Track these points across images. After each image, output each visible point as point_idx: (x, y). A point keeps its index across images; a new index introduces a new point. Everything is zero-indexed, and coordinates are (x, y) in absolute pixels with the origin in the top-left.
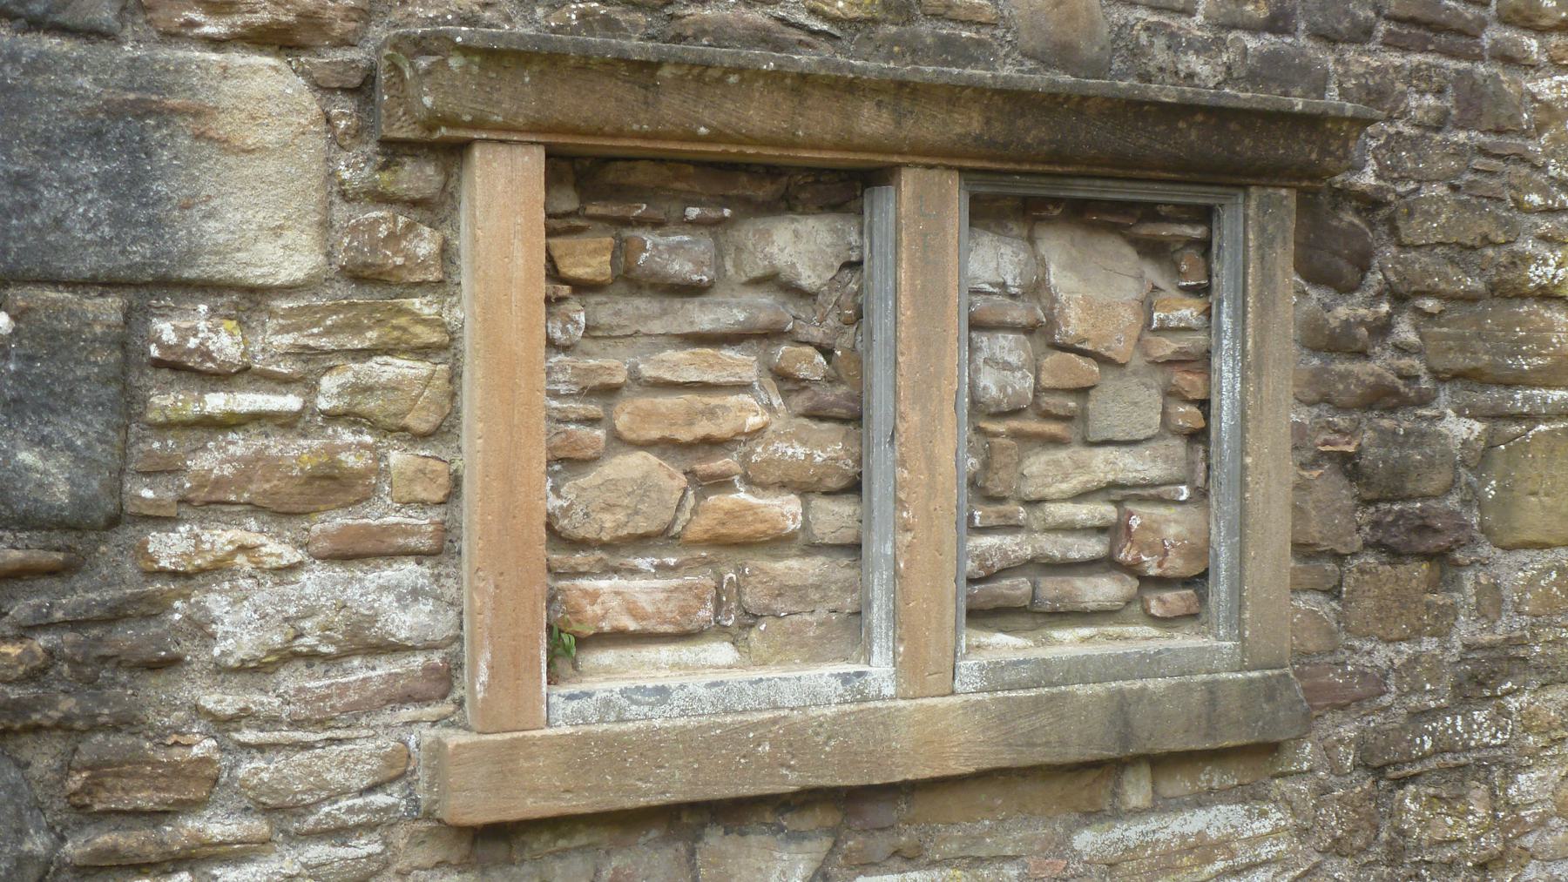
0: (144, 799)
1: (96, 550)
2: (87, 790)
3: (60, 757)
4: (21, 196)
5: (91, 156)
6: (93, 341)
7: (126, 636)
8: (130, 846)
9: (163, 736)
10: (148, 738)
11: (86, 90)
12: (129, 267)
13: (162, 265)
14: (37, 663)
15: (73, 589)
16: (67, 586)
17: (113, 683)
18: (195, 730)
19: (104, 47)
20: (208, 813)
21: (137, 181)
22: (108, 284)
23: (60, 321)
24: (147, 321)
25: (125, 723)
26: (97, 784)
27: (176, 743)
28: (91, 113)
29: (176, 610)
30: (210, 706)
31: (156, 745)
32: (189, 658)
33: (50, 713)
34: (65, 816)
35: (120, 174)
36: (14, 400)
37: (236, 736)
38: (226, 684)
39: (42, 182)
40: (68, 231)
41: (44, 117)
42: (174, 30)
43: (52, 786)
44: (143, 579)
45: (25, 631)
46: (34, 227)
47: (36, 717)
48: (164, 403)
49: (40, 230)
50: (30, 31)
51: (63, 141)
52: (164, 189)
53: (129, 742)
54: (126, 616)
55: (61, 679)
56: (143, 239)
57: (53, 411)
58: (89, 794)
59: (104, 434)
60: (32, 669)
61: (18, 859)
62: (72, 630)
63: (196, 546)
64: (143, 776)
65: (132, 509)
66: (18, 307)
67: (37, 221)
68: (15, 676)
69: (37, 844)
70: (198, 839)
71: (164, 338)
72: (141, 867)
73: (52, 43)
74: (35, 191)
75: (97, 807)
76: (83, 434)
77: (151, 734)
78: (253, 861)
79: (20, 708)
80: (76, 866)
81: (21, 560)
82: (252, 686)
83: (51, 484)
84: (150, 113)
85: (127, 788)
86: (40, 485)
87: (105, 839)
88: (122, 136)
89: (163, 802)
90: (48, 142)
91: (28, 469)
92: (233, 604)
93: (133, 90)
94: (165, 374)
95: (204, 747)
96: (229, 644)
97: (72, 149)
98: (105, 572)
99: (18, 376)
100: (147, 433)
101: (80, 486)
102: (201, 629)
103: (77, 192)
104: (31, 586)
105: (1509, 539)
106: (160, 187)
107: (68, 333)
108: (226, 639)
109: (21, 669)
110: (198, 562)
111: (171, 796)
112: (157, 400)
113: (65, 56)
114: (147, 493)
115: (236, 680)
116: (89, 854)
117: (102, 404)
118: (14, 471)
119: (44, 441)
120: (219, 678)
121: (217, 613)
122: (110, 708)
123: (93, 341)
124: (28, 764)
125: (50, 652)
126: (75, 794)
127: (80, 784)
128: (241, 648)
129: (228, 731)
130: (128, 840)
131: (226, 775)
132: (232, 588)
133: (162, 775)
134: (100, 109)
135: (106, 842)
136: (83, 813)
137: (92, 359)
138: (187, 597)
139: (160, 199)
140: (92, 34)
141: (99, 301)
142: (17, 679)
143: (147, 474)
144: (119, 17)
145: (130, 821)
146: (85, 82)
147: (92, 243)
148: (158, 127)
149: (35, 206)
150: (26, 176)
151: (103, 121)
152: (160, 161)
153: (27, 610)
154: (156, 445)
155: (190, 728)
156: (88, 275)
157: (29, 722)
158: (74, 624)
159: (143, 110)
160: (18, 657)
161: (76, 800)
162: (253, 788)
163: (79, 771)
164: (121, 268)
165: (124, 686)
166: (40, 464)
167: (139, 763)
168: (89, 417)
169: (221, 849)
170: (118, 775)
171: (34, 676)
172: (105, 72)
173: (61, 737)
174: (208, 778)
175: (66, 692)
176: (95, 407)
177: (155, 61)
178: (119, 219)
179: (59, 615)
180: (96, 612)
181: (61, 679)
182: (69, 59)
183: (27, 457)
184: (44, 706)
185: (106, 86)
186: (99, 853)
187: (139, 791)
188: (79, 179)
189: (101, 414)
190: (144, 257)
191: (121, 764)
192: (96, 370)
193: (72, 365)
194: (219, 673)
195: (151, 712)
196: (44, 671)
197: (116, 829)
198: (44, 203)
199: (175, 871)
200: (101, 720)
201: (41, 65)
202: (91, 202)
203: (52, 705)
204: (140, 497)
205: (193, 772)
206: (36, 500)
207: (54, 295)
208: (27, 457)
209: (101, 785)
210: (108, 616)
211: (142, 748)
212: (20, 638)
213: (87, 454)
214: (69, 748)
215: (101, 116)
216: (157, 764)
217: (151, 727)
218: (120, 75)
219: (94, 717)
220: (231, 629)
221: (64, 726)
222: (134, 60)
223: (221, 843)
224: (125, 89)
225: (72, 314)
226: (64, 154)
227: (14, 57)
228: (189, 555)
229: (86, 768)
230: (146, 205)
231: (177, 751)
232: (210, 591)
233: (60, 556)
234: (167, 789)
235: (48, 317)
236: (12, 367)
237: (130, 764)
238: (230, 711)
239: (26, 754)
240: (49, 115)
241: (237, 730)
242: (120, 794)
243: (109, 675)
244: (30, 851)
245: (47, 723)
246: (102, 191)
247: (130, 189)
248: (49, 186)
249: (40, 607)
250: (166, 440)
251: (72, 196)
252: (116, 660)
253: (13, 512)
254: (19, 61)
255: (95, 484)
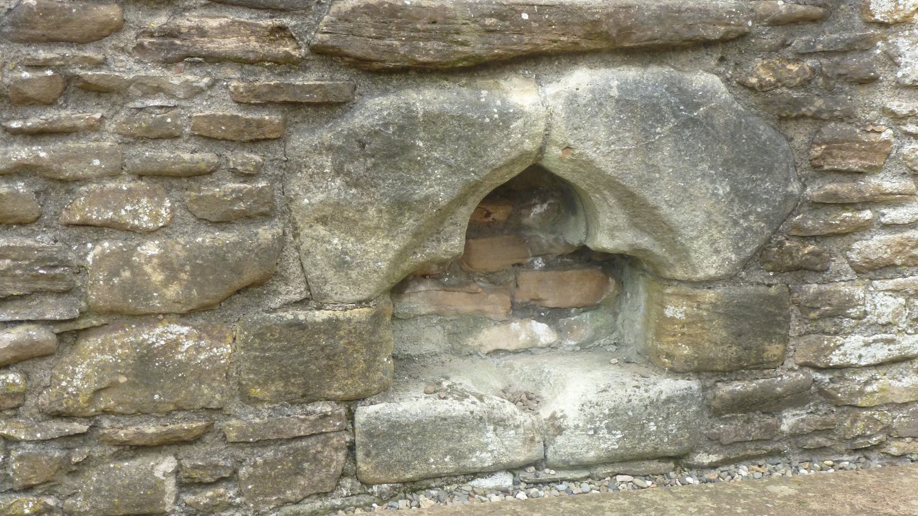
0: (854, 164)
1: (838, 7)
3: (808, 136)
7: (853, 62)
15: (824, 32)
16: (820, 30)
17: (842, 91)
18: (882, 123)
20: (881, 175)
25: (848, 117)
27: (873, 131)
30: (894, 108)
31: (862, 131)
32: (881, 78)
33: (811, 108)
34: (807, 172)
37: (904, 128)
38: (900, 95)
43: (803, 153)
44: (865, 26)
45: (800, 56)
47: (804, 110)
53: (848, 128)
54: (855, 50)
60: (804, 80)
61: (786, 196)
63: (895, 7)
64: (854, 150)
68: (795, 84)
70: (879, 190)
75: (826, 167)
78: (903, 206)
80: (813, 202)
81: (804, 11)
82: (914, 97)
85: (844, 156)
87: (831, 187)
89: (863, 166)
92: (911, 45)
95: (887, 134)
96: (907, 70)
102: (892, 60)
108: (906, 67)
109: (798, 79)
110: (896, 17)
111: (867, 163)
115: (906, 93)
116: (822, 196)
120: (897, 91)
121: (902, 50)
122: (841, 107)
124: (792, 139)
125: (813, 70)
127: (820, 152)
128: (914, 73)
129: (899, 124)
130: (842, 188)
131: (895, 152)
132: (910, 34)
133: (864, 150)
135: (832, 189)
136: (818, 171)
138: (885, 40)
142: (796, 86)
145: (841, 177)
153: (801, 43)
155: (879, 121)
157: (800, 113)
158: (826, 53)
160: (797, 72)
161: (816, 162)
162: (911, 161)
163: (819, 145)
165: (846, 94)
169: (889, 197)
170: (840, 149)
171: (805, 84)
173: (811, 123)
174: (885, 153)
175: (818, 95)
179: (819, 47)
180: (840, 46)
184: (808, 103)
186: (828, 195)
187: (851, 159)
191: (843, 142)
194: (897, 88)
195: (859, 110)
196: (809, 82)
197: (833, 182)
199: (863, 209)
200: (836, 113)
203: (811, 103)
205: (880, 149)
209: (830, 154)
210: (846, 49)
211: (855, 132)
212: (796, 61)
214: (814, 131)
216: (862, 142)
220: (909, 60)
221: (816, 118)
223: (891, 194)
228: (891, 12)
231: (872, 135)
232: (897, 36)
233: (821, 10)
237: (848, 142)
238: (905, 112)
239: (790, 133)
241: (905, 125)
242: (839, 160)
244: (792, 192)
245: (809, 114)
249: (809, 41)
252: (844, 77)
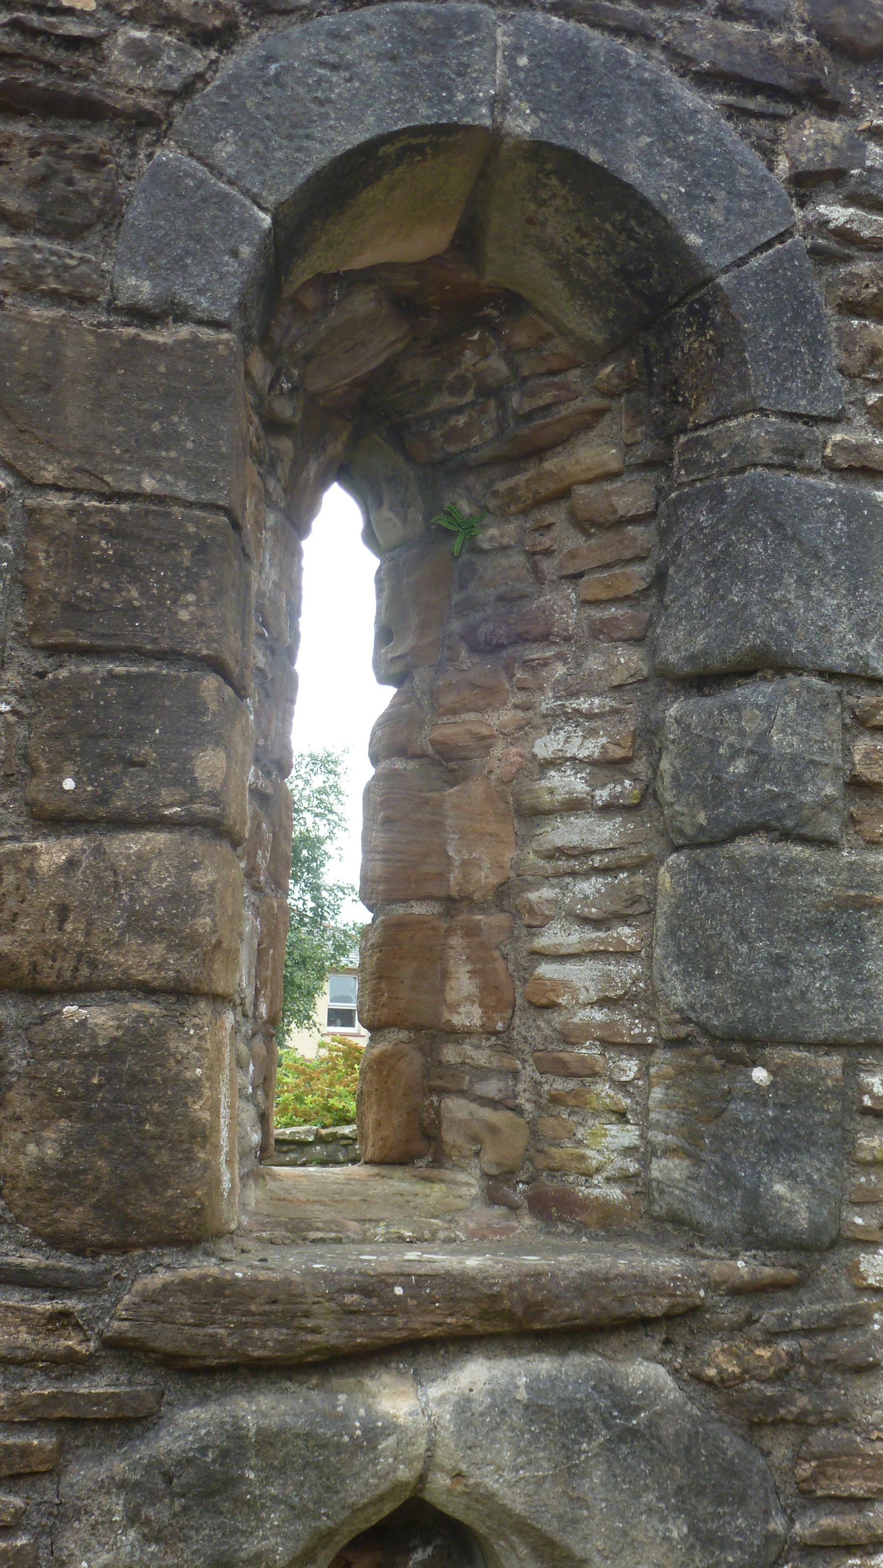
0: (857, 1487)
1: (818, 1268)
2: (813, 1478)
4: (779, 974)
5: (825, 941)
6: (826, 1092)
8: (846, 1529)
9: (867, 1432)
10: (857, 1433)
11: (822, 888)
12: (850, 1031)
13: (872, 1030)
14: (784, 1364)
19: (831, 853)
21: (856, 960)
22: (831, 1045)
23: (804, 1076)
24: (856, 1075)
25: (843, 1420)
26: (820, 1473)
28: (826, 905)
29: (875, 1322)
31: (864, 1439)
35: (844, 955)
36: (772, 1141)
39: (792, 962)
40: (809, 1002)
41: (795, 910)
42: (876, 839)
43: (786, 1473)
44: (854, 1294)
45: (771, 1337)
46: (787, 999)
47: (782, 1412)
48: (872, 1144)
49: (791, 1001)
50: (781, 840)
51: (807, 929)
52: (873, 968)
53: (845, 1436)
55: (798, 1379)
56: (861, 1009)
57: (798, 1150)
58: (815, 1481)
59: (833, 1170)
60: (780, 1370)
62: (805, 1337)
64: (856, 1466)
65: (849, 1234)
66: (776, 1064)
67: (789, 993)
69: (777, 1524)
71: (875, 1090)
72: (851, 1547)
73: (797, 850)
74: (787, 969)
75: (819, 1493)
76: (819, 1170)
77: (859, 1429)
79: (771, 1404)
80: (805, 1545)
81: (772, 1275)
83: (796, 1212)
84: (864, 906)
86: (789, 1212)
87: (828, 1522)
88: (845, 925)
89: (869, 1490)
90: (797, 930)
91: (781, 1198)
93: (852, 887)
94: (870, 1120)
97: (813, 936)
98: (825, 1287)
99: (775, 1120)
100: (856, 1169)
101: (815, 1214)
103: (816, 969)
104: (772, 1298)
105: (425, 761)
106: (870, 966)
107: (809, 1085)
109: (772, 1369)
112: (864, 1141)
113: (807, 860)
114: (859, 1221)
117: (832, 1145)
118: (770, 1200)
119: (792, 1176)
122: (832, 1406)
123: (826, 1092)
125: (791, 1355)
126: (804, 1481)
127: (809, 1472)
133: (869, 1466)
134: (832, 902)
135: (829, 1525)
137: (825, 1107)
139: (871, 975)
140: (827, 843)
141: (826, 1058)
143: (857, 1204)
144: (841, 830)
146: (820, 881)
147: (826, 1012)
148: (869, 918)
149: (788, 982)
150: (783, 958)
151: (833, 913)
152: (871, 945)
154: (863, 1180)
156: (822, 1037)
158: (807, 1332)
159: (861, 904)
160: (769, 1359)
161: (804, 1486)
163: (807, 1461)
164: (846, 1032)
166: (788, 1195)
167: (853, 1455)
168: (823, 1156)
170: (836, 1465)
171: (781, 1376)
172: (832, 873)
176: (827, 1147)
177: (867, 864)
178: (844, 992)
179: (797, 1323)
180: (825, 1322)
181: (798, 1379)
182: (809, 863)
183: (780, 1188)
185: (835, 885)
187: (852, 1479)
188: (817, 959)
189: (831, 1153)
190: (861, 1024)
192: (828, 1116)
193: (811, 1111)
195: (858, 1409)
198: (794, 979)
200: (827, 1416)
201: (791, 869)
202: (825, 978)
203: (792, 1402)
204: (854, 1223)
206: (785, 1225)
207: (798, 1054)
208: (780, 1188)
210: (832, 1325)
213: (821, 1187)
215: (832, 909)
217: (859, 1424)
218: (844, 876)
219: (822, 1413)
221: (800, 1422)
222: (851, 863)
224: (847, 887)
225: (811, 1070)
226: (807, 939)
227: (774, 862)
229: (815, 1458)
230: (861, 981)
233: (795, 1273)
234: (871, 1479)
235: (795, 1072)
236: (770, 1113)
237: (846, 1455)
239: (767, 1444)
240: (798, 908)
242: (837, 1482)
243: (828, 1376)
244: (775, 1530)
246: (831, 969)
247: (850, 968)
248: (797, 965)
249: (783, 1316)
250: (869, 1175)
251: (812, 973)
253: (768, 1234)
254: (777, 865)
255: (825, 1212)
